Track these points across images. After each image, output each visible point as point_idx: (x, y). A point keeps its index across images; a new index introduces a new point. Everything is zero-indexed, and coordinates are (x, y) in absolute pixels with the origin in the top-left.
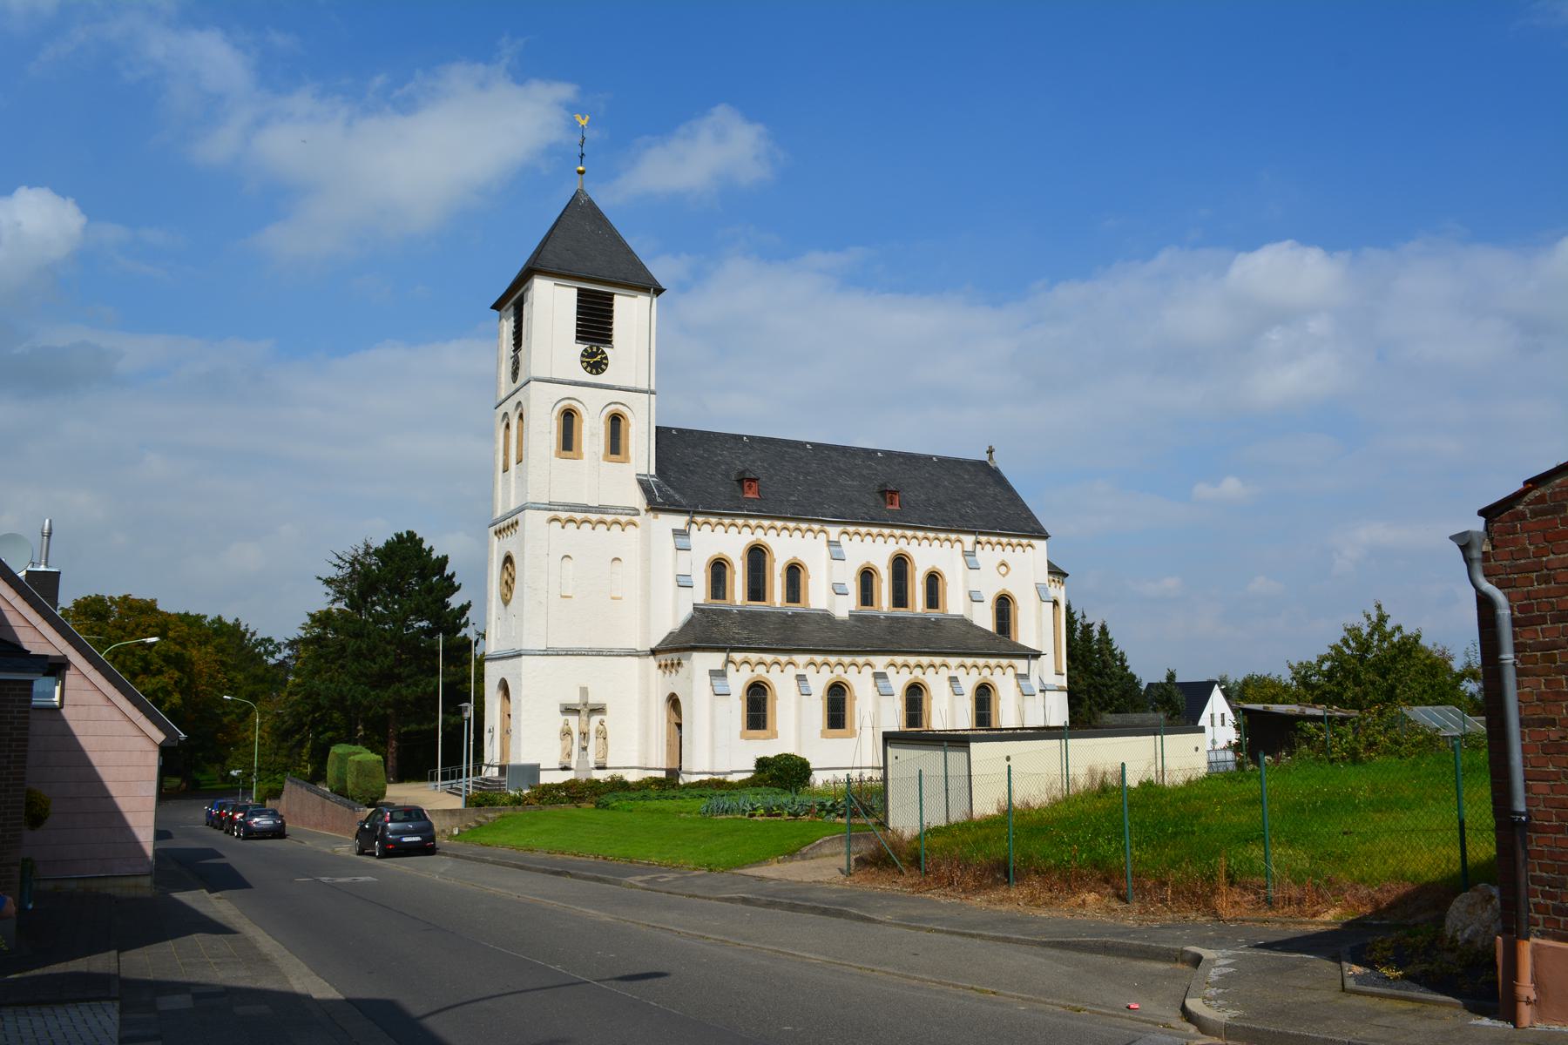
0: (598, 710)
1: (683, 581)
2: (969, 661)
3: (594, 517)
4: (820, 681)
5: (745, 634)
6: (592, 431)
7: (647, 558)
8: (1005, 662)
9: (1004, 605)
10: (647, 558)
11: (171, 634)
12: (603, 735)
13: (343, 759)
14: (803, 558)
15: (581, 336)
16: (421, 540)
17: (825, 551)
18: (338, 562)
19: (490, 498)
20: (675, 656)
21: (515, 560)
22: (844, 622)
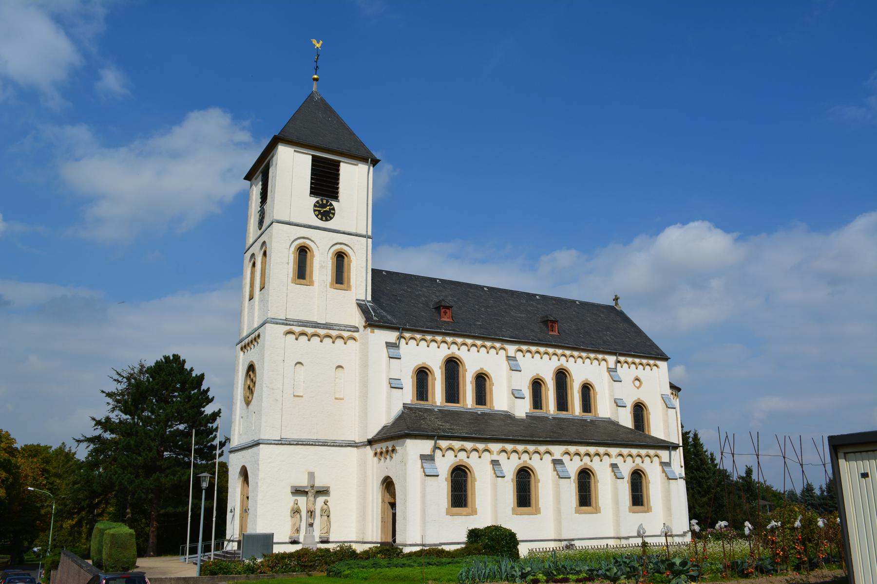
0: (323, 492)
1: (394, 383)
3: (322, 332)
4: (510, 466)
5: (447, 426)
6: (321, 265)
7: (365, 365)
8: (652, 452)
9: (639, 410)
10: (365, 365)
12: (326, 513)
13: (102, 532)
14: (488, 369)
15: (314, 192)
16: (184, 361)
17: (505, 364)
18: (117, 377)
19: (238, 315)
20: (389, 444)
21: (257, 367)
22: (522, 420)
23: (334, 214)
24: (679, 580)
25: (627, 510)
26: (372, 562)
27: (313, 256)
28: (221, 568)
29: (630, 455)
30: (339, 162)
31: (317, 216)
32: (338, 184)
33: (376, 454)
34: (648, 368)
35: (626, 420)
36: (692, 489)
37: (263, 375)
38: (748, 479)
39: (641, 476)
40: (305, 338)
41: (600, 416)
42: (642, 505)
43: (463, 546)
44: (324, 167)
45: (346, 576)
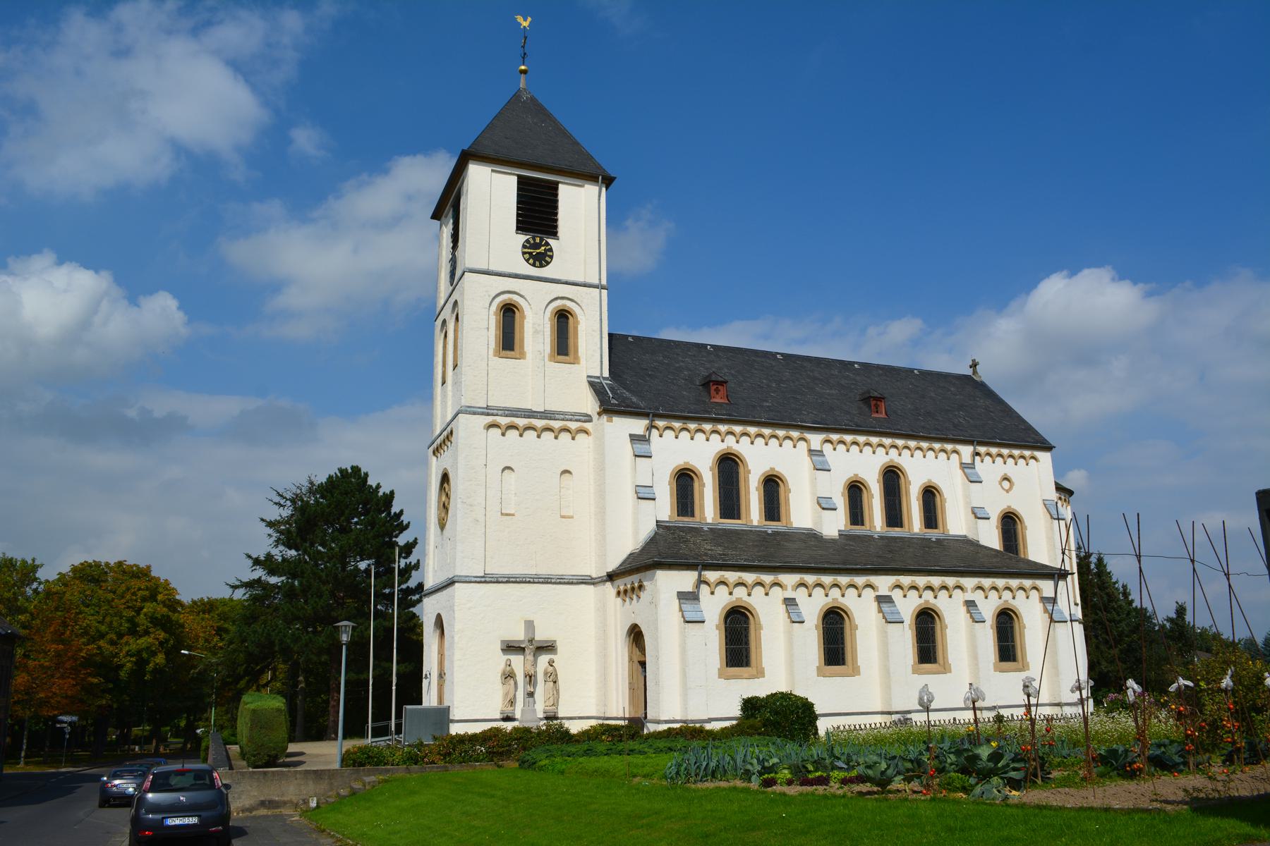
0: (547, 647)
2: (987, 582)
3: (539, 423)
4: (813, 606)
5: (719, 550)
6: (536, 330)
8: (1027, 583)
9: (1010, 523)
11: (160, 597)
15: (521, 227)
16: (366, 475)
17: (806, 462)
18: (277, 499)
20: (635, 578)
22: (833, 541)
23: (551, 257)
24: (987, 786)
25: (992, 666)
26: (586, 747)
27: (523, 317)
28: (369, 757)
29: (995, 588)
30: (557, 183)
31: (527, 261)
32: (556, 214)
33: (619, 593)
34: (1021, 461)
35: (991, 537)
36: (1096, 637)
37: (458, 485)
38: (1180, 622)
39: (1011, 618)
40: (516, 433)
41: (951, 533)
42: (1014, 660)
43: (734, 722)
44: (535, 192)
45: (541, 768)
